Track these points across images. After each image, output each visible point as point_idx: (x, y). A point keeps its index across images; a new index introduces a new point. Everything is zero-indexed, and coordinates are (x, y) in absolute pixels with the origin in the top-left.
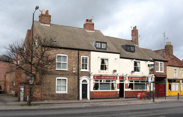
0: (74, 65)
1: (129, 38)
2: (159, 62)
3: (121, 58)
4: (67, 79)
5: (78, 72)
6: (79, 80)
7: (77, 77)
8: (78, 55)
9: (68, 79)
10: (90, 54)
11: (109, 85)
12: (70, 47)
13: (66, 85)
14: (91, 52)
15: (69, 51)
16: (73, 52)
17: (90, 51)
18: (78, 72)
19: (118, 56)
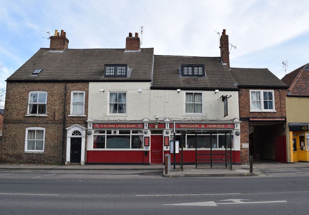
0: (57, 108)
1: (217, 53)
2: (262, 91)
3: (152, 88)
4: (44, 129)
5: (64, 118)
6: (65, 132)
7: (61, 127)
9: (46, 130)
10: (88, 88)
11: (128, 139)
12: (52, 79)
14: (91, 84)
15: (49, 85)
17: (88, 81)
18: (64, 118)
19: (148, 85)
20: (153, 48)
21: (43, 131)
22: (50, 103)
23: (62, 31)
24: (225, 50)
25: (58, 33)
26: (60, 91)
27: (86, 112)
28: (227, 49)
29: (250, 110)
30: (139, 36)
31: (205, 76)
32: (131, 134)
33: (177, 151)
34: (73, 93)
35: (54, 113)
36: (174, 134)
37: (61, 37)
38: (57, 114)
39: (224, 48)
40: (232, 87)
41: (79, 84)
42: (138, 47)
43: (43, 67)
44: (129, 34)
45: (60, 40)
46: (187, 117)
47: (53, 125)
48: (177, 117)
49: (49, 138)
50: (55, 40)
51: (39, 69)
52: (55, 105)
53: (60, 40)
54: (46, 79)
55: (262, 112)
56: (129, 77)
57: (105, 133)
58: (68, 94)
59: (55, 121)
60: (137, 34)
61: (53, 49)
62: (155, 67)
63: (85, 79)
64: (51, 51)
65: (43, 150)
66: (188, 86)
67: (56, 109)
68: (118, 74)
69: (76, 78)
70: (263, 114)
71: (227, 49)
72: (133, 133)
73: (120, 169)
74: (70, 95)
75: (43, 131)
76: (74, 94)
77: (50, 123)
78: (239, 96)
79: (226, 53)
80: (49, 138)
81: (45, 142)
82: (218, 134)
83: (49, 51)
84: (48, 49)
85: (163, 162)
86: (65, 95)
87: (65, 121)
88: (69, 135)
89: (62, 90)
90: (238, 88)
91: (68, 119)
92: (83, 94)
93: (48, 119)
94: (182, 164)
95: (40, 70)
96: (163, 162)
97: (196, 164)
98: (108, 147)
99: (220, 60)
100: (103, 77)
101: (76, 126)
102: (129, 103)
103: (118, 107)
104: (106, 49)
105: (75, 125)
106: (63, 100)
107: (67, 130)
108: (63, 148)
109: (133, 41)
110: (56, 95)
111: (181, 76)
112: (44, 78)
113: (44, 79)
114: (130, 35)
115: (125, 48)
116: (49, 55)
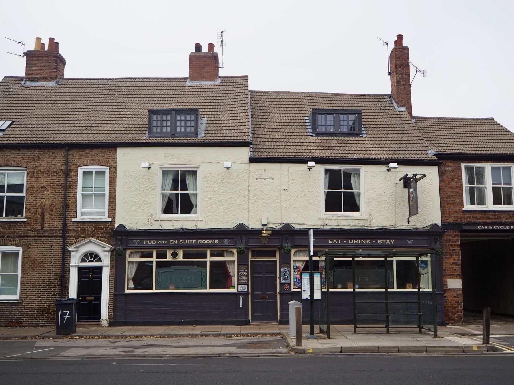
0: (48, 203)
1: (379, 82)
2: (488, 167)
3: (253, 160)
4: (20, 250)
5: (65, 225)
6: (66, 256)
7: (57, 244)
8: (67, 163)
9: (23, 252)
10: (115, 159)
11: (202, 270)
12: (35, 140)
13: (16, 271)
14: (121, 152)
15: (29, 153)
16: (45, 157)
17: (114, 146)
18: (65, 225)
19: (245, 153)
20: (247, 76)
21: (16, 254)
22: (31, 194)
23: (51, 40)
24: (403, 78)
25: (43, 45)
26: (53, 166)
27: (112, 212)
28: (406, 76)
29: (463, 206)
30: (217, 50)
31: (362, 134)
32: (209, 259)
33: (317, 296)
34: (163, 171)
35: (43, 216)
36: (311, 257)
37: (50, 52)
38: (47, 217)
39: (400, 74)
40: (423, 157)
41: (95, 152)
42: (216, 75)
43: (13, 117)
44: (195, 46)
45: (45, 60)
46: (328, 221)
47: (39, 241)
48: (305, 222)
49: (31, 270)
50: (36, 59)
51: (6, 120)
52: (44, 196)
53: (45, 60)
54: (23, 142)
55: (490, 211)
56: (203, 135)
57: (152, 257)
58: (72, 174)
59: (44, 232)
60: (211, 46)
61: (32, 78)
62: (255, 116)
63: (110, 139)
64: (28, 84)
65: (16, 294)
66: (327, 154)
67: (46, 207)
68: (179, 130)
69: (93, 139)
70: (492, 216)
71: (406, 76)
72: (212, 255)
73: (202, 335)
74: (77, 175)
75: (16, 254)
76: (85, 173)
77: (33, 237)
78: (441, 176)
79: (404, 85)
80: (31, 270)
81: (22, 277)
82: (395, 259)
83: (23, 82)
84: (21, 79)
85: (278, 318)
86: (67, 175)
87: (68, 232)
88: (75, 260)
89: (59, 166)
90: (436, 158)
91: (71, 228)
92: (103, 172)
93: (28, 228)
94: (328, 323)
95: (8, 123)
96: (278, 318)
97: (387, 322)
98: (158, 286)
99: (391, 101)
100: (147, 135)
101: (90, 242)
102: (201, 190)
103: (180, 200)
104: (147, 78)
105: (87, 240)
106: (60, 187)
107: (69, 252)
108: (62, 291)
109: (204, 62)
110: (46, 175)
111: (311, 134)
112: (19, 139)
113: (18, 141)
114: (198, 47)
115: (188, 76)
116: (24, 91)
